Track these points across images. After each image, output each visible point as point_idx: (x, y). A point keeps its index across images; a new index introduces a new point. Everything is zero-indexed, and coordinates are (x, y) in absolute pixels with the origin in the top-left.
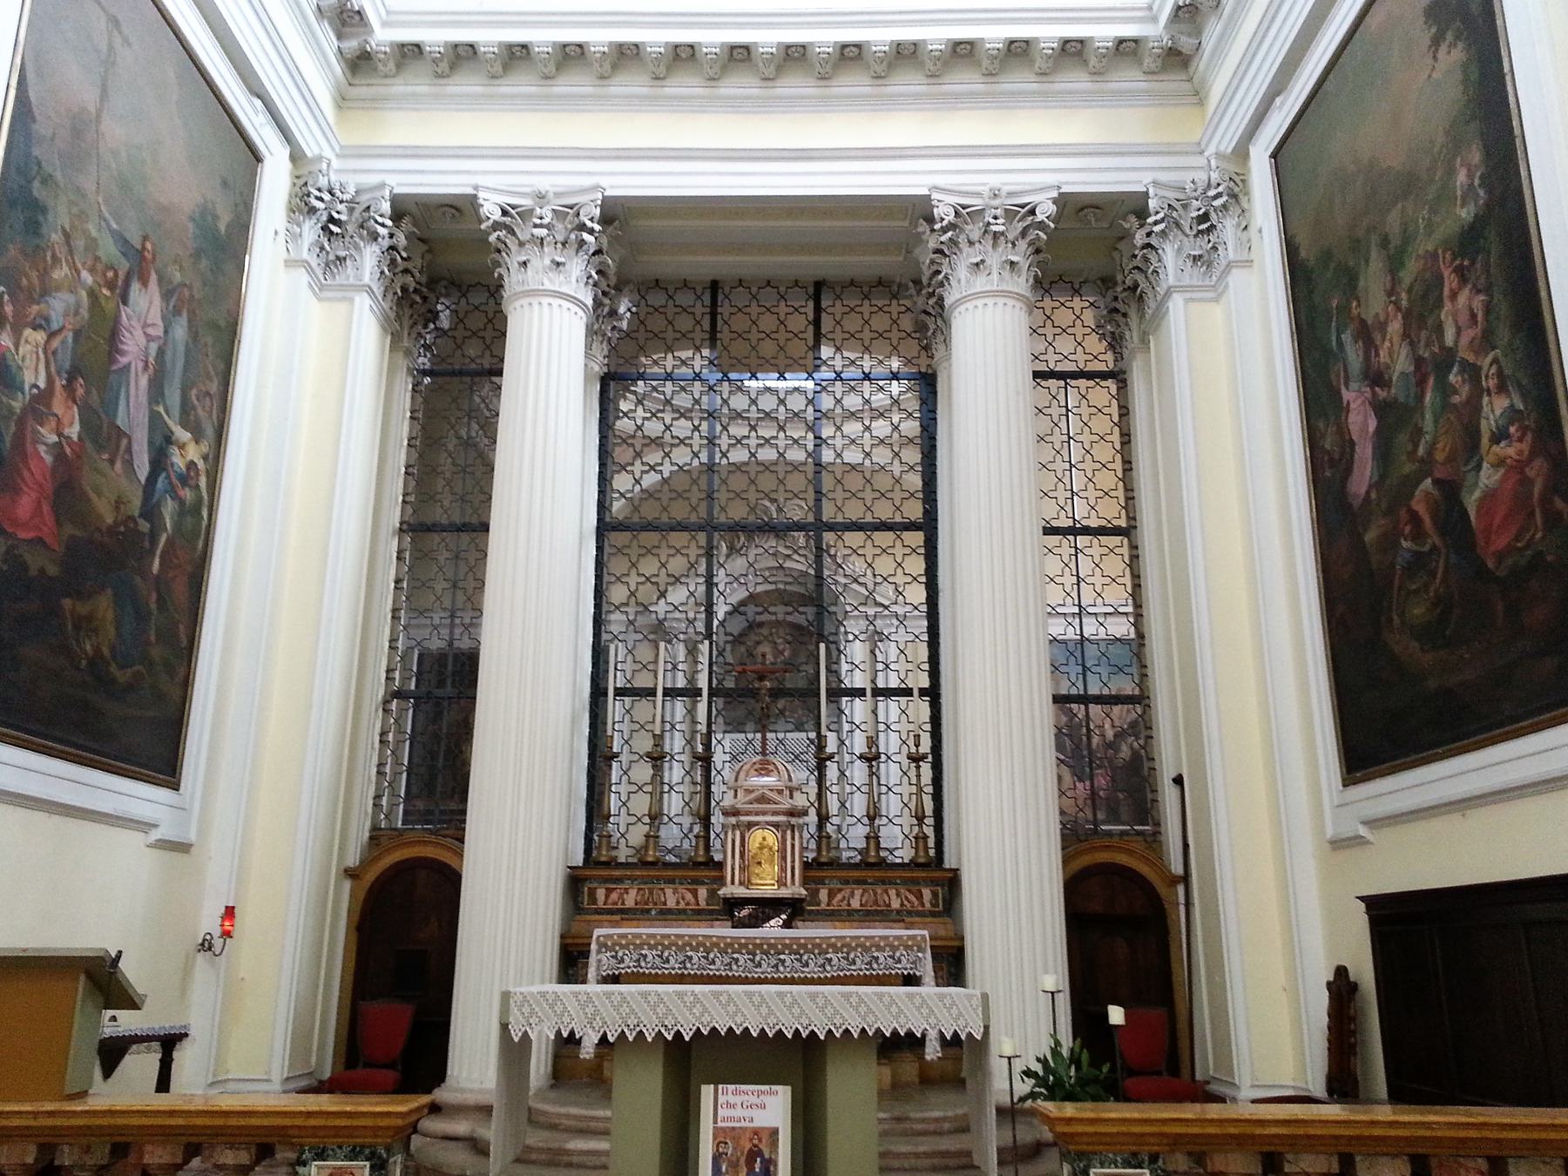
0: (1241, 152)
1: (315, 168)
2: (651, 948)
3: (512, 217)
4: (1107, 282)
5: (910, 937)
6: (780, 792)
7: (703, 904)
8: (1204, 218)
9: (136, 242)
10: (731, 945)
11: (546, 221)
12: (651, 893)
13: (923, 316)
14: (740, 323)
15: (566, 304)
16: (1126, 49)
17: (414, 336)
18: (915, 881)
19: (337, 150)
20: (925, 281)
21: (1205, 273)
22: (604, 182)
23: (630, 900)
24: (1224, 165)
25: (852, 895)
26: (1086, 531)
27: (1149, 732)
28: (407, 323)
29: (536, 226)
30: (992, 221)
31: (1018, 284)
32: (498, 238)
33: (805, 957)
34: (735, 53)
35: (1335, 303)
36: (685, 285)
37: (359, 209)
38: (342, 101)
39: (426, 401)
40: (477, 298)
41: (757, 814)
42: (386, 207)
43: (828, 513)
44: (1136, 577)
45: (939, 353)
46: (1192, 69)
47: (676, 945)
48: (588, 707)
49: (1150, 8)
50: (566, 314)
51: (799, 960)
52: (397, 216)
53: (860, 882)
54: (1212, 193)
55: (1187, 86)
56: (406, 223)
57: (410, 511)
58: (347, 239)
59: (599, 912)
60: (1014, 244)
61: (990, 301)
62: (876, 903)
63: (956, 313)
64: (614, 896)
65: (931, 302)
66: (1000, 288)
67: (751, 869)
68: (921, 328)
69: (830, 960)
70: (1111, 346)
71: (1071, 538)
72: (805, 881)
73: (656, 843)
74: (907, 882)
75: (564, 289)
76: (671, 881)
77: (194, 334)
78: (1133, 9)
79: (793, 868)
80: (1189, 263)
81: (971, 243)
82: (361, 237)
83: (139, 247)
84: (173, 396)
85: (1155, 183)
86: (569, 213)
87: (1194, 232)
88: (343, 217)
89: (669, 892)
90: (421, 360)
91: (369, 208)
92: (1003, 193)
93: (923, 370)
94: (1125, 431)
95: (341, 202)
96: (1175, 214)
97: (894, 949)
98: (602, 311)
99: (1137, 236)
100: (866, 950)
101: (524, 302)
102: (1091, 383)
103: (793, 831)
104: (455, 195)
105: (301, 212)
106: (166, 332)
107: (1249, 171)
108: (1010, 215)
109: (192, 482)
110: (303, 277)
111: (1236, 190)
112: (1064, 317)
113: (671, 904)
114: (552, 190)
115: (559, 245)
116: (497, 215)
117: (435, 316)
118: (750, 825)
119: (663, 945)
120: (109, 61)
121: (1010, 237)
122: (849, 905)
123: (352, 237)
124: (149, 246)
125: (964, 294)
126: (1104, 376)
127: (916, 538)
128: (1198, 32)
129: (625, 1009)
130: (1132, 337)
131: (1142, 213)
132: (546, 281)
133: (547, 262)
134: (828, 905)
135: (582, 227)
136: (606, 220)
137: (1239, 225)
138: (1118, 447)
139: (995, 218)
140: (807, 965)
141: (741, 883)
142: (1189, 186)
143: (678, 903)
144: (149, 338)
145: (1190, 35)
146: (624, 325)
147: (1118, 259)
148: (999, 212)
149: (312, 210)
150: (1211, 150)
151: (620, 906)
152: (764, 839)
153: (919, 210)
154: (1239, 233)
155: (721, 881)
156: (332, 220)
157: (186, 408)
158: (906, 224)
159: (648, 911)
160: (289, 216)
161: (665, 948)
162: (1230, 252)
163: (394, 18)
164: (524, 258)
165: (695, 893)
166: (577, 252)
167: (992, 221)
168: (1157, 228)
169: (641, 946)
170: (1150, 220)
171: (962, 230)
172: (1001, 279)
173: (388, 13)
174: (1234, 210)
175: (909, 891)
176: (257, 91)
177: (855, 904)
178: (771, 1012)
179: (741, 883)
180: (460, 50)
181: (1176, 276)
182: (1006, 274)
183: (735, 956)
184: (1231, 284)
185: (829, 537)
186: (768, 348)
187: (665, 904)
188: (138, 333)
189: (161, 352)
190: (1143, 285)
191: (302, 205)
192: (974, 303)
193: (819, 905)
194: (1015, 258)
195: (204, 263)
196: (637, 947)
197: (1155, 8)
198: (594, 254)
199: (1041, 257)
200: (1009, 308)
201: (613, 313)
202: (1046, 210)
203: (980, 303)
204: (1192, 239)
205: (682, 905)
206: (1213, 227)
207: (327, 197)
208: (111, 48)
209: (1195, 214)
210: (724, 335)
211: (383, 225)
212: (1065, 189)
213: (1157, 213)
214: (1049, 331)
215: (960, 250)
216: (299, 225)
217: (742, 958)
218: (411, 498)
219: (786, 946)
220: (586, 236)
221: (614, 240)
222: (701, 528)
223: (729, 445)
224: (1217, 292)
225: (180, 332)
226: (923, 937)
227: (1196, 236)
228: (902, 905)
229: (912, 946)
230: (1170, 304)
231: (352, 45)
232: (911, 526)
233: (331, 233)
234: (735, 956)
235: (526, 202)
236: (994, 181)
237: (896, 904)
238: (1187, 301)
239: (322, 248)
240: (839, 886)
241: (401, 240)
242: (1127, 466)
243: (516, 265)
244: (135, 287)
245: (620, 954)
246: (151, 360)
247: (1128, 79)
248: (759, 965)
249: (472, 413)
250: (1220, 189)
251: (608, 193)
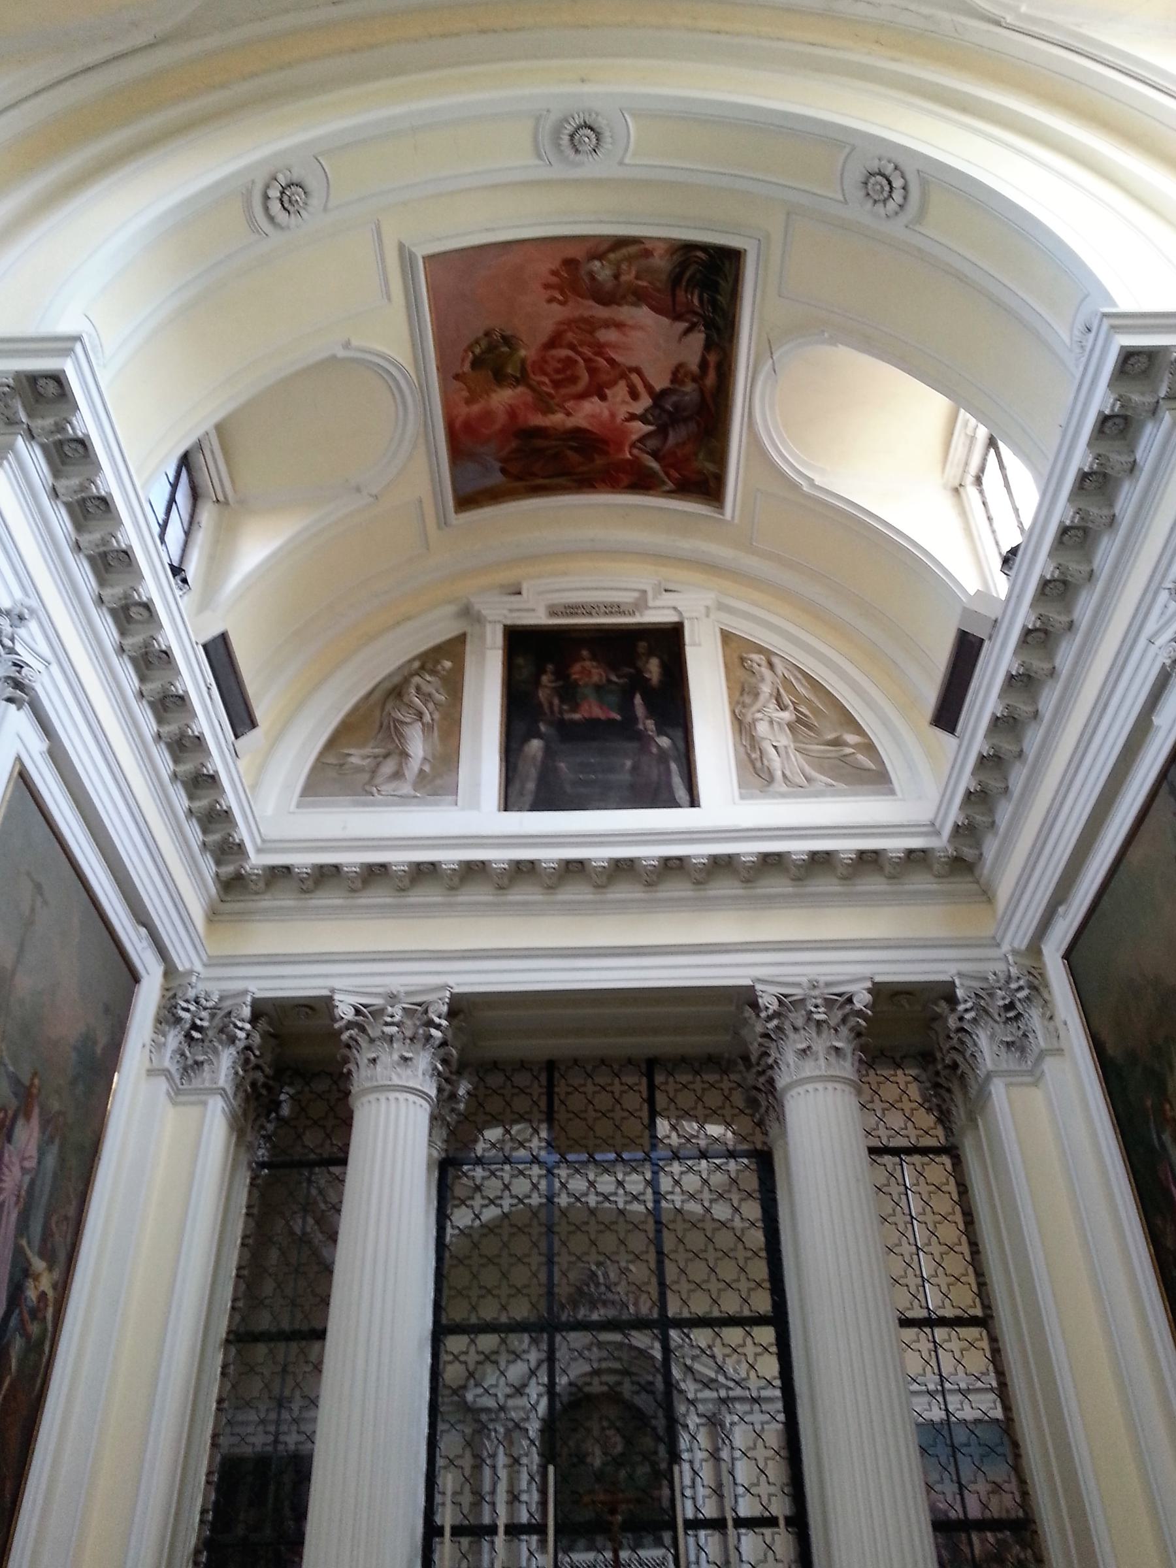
0: (1034, 949)
1: (185, 982)
3: (364, 1016)
4: (926, 1058)
8: (1010, 1006)
9: (26, 1080)
11: (397, 1019)
13: (754, 1092)
14: (576, 1102)
15: (412, 1098)
16: (915, 858)
17: (256, 1128)
19: (205, 958)
20: (754, 1059)
21: (1020, 1058)
22: (451, 980)
24: (1018, 959)
26: (943, 1322)
28: (252, 1116)
29: (387, 1024)
30: (813, 1009)
31: (844, 1068)
32: (351, 1037)
34: (570, 866)
35: (1149, 1103)
36: (523, 1065)
37: (221, 1014)
38: (213, 915)
39: (262, 1195)
40: (321, 1086)
42: (246, 1012)
44: (979, 1274)
45: (774, 1130)
46: (977, 873)
48: (420, 1552)
49: (933, 824)
50: (411, 1106)
52: (254, 1019)
54: (1014, 986)
55: (975, 886)
56: (263, 1024)
57: (238, 1317)
58: (207, 1043)
60: (836, 1030)
61: (820, 1086)
63: (788, 1096)
65: (762, 1079)
66: (829, 1073)
68: (753, 1103)
70: (940, 1120)
71: (928, 1330)
75: (411, 1084)
77: (62, 1160)
78: (919, 826)
80: (1003, 1049)
81: (796, 1029)
82: (221, 1042)
83: (27, 1083)
84: (36, 1228)
85: (960, 975)
86: (419, 1012)
88: (205, 1024)
90: (260, 1152)
91: (230, 1013)
92: (822, 984)
93: (759, 1146)
95: (205, 1009)
96: (982, 1003)
98: (445, 1098)
101: (372, 1097)
102: (926, 1159)
104: (310, 997)
105: (167, 1023)
106: (39, 1163)
107: (1044, 964)
108: (829, 1003)
109: (40, 1315)
110: (162, 1084)
111: (1036, 982)
112: (890, 1092)
114: (402, 989)
115: (408, 1041)
116: (349, 1015)
117: (278, 1104)
120: (29, 923)
121: (832, 1023)
123: (211, 1041)
124: (36, 1081)
126: (937, 1151)
127: (766, 1335)
128: (978, 844)
130: (959, 1114)
131: (952, 1000)
132: (394, 1077)
133: (396, 1057)
135: (430, 1023)
136: (452, 1014)
137: (1043, 1015)
138: (955, 1197)
139: (816, 1006)
142: (991, 977)
144: (24, 1171)
145: (971, 847)
146: (462, 1106)
147: (934, 1038)
148: (819, 1001)
149: (179, 1020)
150: (1006, 947)
153: (746, 997)
154: (1046, 1023)
156: (194, 1027)
157: (47, 1234)
158: (733, 1008)
160: (156, 1027)
162: (1040, 1040)
163: (269, 845)
164: (374, 1055)
166: (424, 1045)
167: (813, 1009)
168: (968, 1016)
170: (961, 1007)
171: (786, 1017)
172: (829, 1064)
173: (264, 841)
174: (1038, 1002)
176: (142, 917)
180: (325, 870)
181: (993, 1060)
182: (833, 1059)
184: (1046, 1071)
186: (603, 1128)
188: (16, 1170)
189: (32, 1183)
190: (963, 1067)
191: (168, 1016)
194: (838, 1044)
195: (80, 1089)
197: (937, 824)
198: (439, 1047)
199: (863, 1040)
200: (839, 1092)
201: (453, 1096)
202: (862, 999)
203: (810, 1087)
206: (1019, 1016)
207: (193, 1008)
208: (33, 910)
209: (1001, 1003)
210: (561, 1115)
211: (241, 1029)
212: (878, 979)
214: (878, 1106)
215: (785, 1035)
216: (164, 1035)
218: (240, 1304)
220: (434, 1032)
221: (458, 1031)
223: (486, 1095)
224: (1036, 1078)
225: (51, 1161)
231: (228, 870)
232: (759, 1320)
233: (192, 1038)
235: (378, 1002)
236: (812, 972)
239: (183, 1055)
241: (257, 1039)
242: (974, 1249)
243: (366, 1061)
244: (20, 1122)
246: (23, 1193)
247: (921, 882)
249: (307, 1208)
250: (1022, 983)
251: (456, 990)
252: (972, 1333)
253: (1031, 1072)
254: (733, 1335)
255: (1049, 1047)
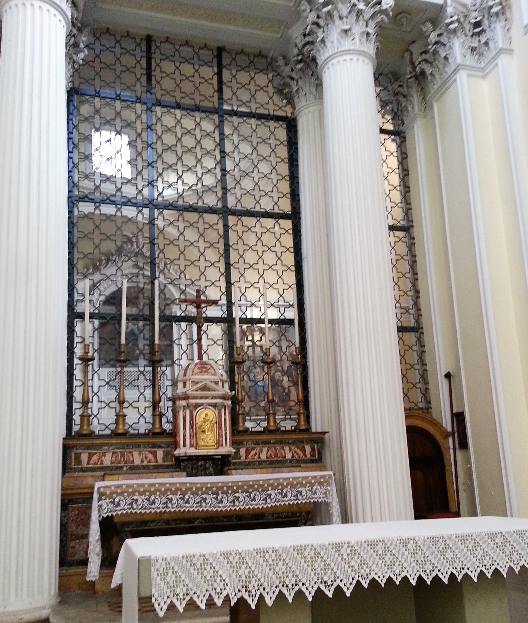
2: (141, 494)
5: (304, 478)
6: (217, 383)
7: (160, 461)
8: (477, 24)
10: (201, 489)
12: (122, 455)
13: (288, 80)
18: (302, 441)
23: (107, 460)
25: (261, 451)
27: (423, 348)
33: (253, 494)
41: (201, 398)
43: (231, 202)
47: (160, 491)
51: (249, 496)
53: (266, 442)
59: (83, 470)
61: (355, 57)
62: (276, 455)
64: (95, 458)
67: (198, 436)
69: (270, 495)
72: (234, 443)
73: (124, 420)
74: (295, 442)
76: (137, 446)
79: (226, 434)
80: (469, 51)
81: (341, 18)
87: (471, 34)
89: (136, 454)
94: (405, 168)
97: (312, 485)
99: (432, 36)
100: (294, 487)
103: (225, 410)
113: (137, 461)
118: (197, 406)
119: (149, 491)
122: (259, 457)
125: (336, 51)
127: (288, 224)
129: (281, 568)
134: (246, 458)
140: (254, 499)
141: (191, 446)
143: (142, 461)
151: (99, 465)
152: (206, 415)
155: (176, 445)
159: (121, 468)
161: (151, 493)
165: (155, 454)
169: (133, 493)
175: (298, 447)
177: (263, 457)
178: (426, 559)
179: (191, 446)
182: (364, 39)
183: (204, 496)
185: (232, 220)
187: (133, 462)
192: (344, 57)
193: (240, 458)
196: (130, 494)
203: (348, 57)
204: (469, 38)
205: (145, 463)
206: (483, 31)
213: (452, 17)
217: (209, 497)
219: (239, 487)
222: (145, 206)
226: (330, 476)
227: (472, 36)
228: (293, 456)
229: (323, 482)
230: (458, 77)
232: (284, 216)
234: (204, 496)
237: (289, 456)
238: (469, 76)
240: (253, 446)
245: (117, 500)
248: (221, 502)
252: (401, 234)
253: (483, 69)
254: (268, 222)
255: (505, 47)
